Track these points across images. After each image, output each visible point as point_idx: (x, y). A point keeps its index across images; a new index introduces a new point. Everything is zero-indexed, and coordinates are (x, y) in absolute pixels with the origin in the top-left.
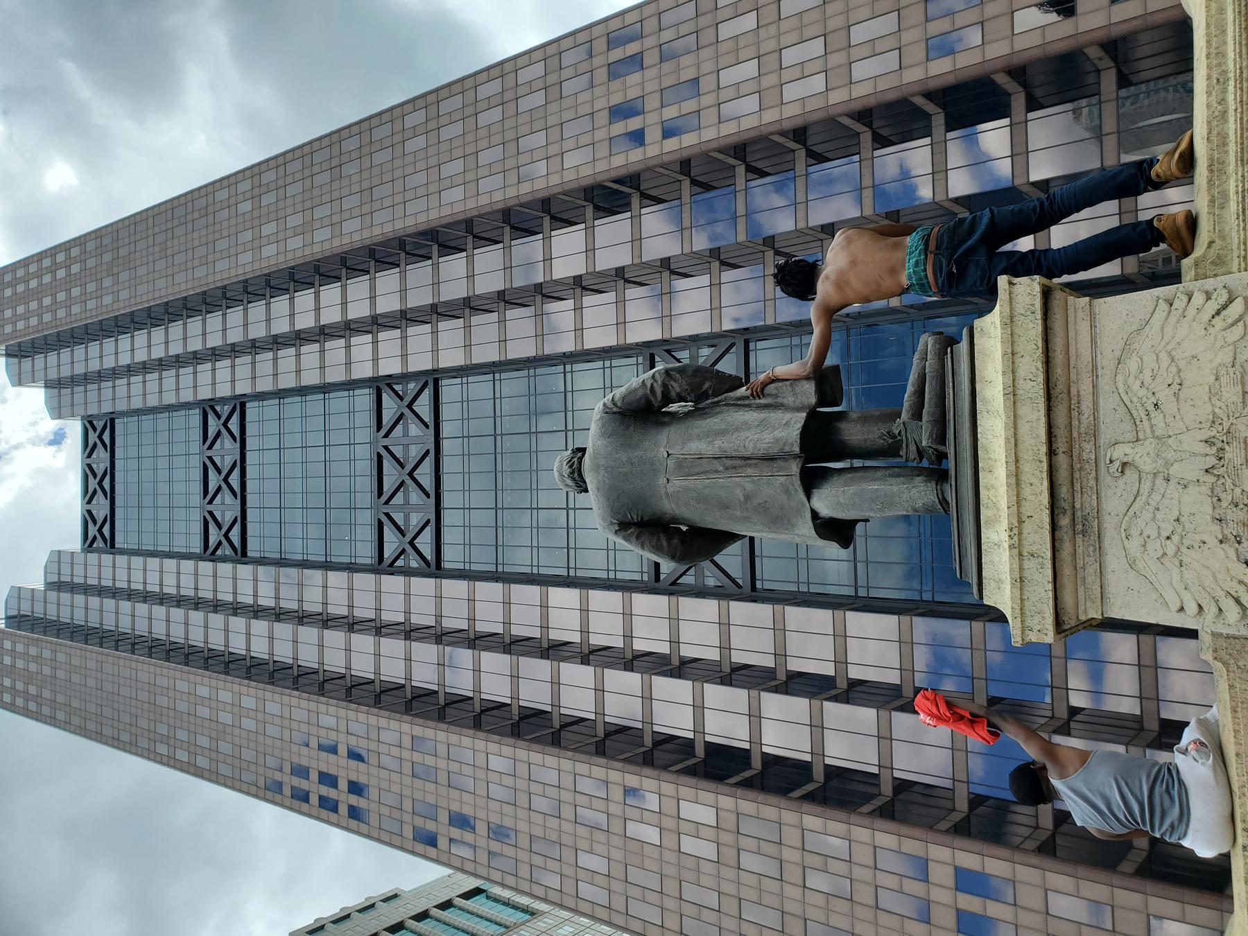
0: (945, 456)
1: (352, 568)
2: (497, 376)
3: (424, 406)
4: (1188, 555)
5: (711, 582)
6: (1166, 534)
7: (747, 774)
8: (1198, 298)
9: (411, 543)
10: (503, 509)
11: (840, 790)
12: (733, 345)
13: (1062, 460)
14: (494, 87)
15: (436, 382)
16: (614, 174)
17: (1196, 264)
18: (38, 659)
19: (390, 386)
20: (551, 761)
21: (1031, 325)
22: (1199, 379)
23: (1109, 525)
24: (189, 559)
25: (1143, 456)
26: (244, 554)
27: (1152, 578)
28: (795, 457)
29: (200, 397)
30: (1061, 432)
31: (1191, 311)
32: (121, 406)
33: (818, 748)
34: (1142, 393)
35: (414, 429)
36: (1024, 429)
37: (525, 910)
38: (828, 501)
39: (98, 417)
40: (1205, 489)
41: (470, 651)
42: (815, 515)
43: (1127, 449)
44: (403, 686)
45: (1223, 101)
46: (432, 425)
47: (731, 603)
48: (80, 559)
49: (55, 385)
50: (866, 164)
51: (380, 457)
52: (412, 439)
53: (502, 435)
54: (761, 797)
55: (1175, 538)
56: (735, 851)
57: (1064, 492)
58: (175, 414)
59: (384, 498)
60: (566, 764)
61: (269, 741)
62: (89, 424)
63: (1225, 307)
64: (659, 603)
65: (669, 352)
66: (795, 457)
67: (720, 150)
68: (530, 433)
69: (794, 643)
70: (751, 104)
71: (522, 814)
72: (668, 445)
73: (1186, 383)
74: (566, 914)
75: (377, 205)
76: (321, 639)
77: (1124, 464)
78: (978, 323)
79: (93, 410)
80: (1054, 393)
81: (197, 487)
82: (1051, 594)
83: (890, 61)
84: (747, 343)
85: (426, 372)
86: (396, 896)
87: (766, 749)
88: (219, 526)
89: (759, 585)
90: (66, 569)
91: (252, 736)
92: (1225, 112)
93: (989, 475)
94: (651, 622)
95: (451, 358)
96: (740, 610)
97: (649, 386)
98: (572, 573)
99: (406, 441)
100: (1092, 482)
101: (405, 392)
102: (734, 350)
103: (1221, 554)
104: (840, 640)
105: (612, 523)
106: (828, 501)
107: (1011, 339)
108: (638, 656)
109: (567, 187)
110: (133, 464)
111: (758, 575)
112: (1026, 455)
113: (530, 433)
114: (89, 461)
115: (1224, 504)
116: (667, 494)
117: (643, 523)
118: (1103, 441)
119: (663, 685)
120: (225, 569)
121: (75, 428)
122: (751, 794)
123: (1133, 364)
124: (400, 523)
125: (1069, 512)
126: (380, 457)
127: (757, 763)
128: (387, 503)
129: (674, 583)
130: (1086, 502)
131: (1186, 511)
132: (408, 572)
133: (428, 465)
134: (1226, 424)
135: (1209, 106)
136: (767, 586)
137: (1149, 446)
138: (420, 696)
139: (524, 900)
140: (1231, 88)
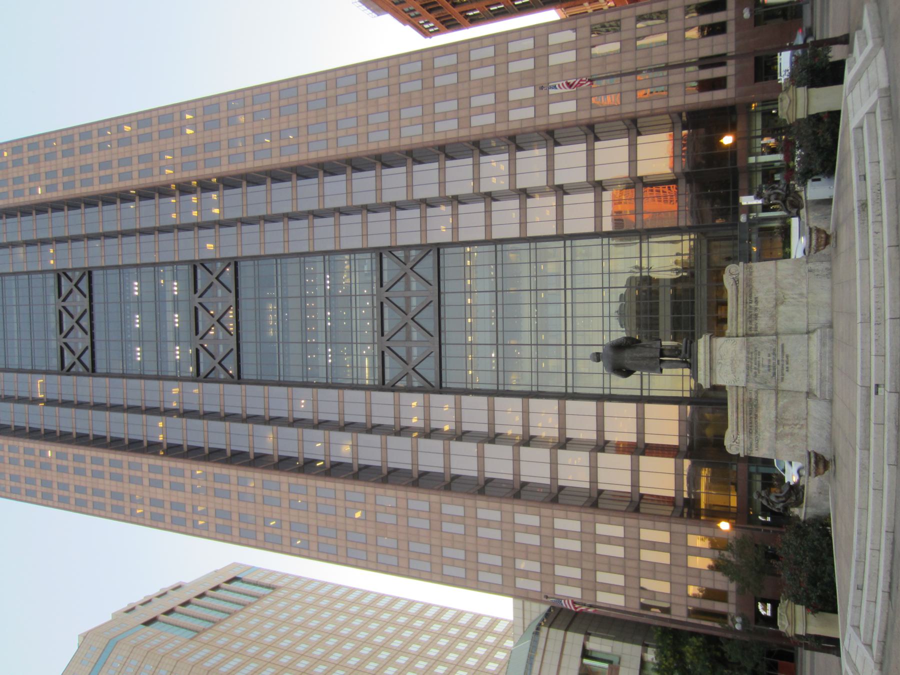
5: (416, 384)
14: (452, 59)
19: (203, 265)
26: (94, 370)
46: (88, 295)
51: (196, 309)
59: (64, 334)
67: (433, 147)
69: (376, 410)
70: (418, 130)
85: (85, 268)
89: (444, 385)
96: (435, 398)
104: (368, 405)
109: (340, 158)
111: (443, 380)
119: (310, 433)
126: (196, 309)
128: (201, 338)
129: (393, 386)
136: (449, 385)
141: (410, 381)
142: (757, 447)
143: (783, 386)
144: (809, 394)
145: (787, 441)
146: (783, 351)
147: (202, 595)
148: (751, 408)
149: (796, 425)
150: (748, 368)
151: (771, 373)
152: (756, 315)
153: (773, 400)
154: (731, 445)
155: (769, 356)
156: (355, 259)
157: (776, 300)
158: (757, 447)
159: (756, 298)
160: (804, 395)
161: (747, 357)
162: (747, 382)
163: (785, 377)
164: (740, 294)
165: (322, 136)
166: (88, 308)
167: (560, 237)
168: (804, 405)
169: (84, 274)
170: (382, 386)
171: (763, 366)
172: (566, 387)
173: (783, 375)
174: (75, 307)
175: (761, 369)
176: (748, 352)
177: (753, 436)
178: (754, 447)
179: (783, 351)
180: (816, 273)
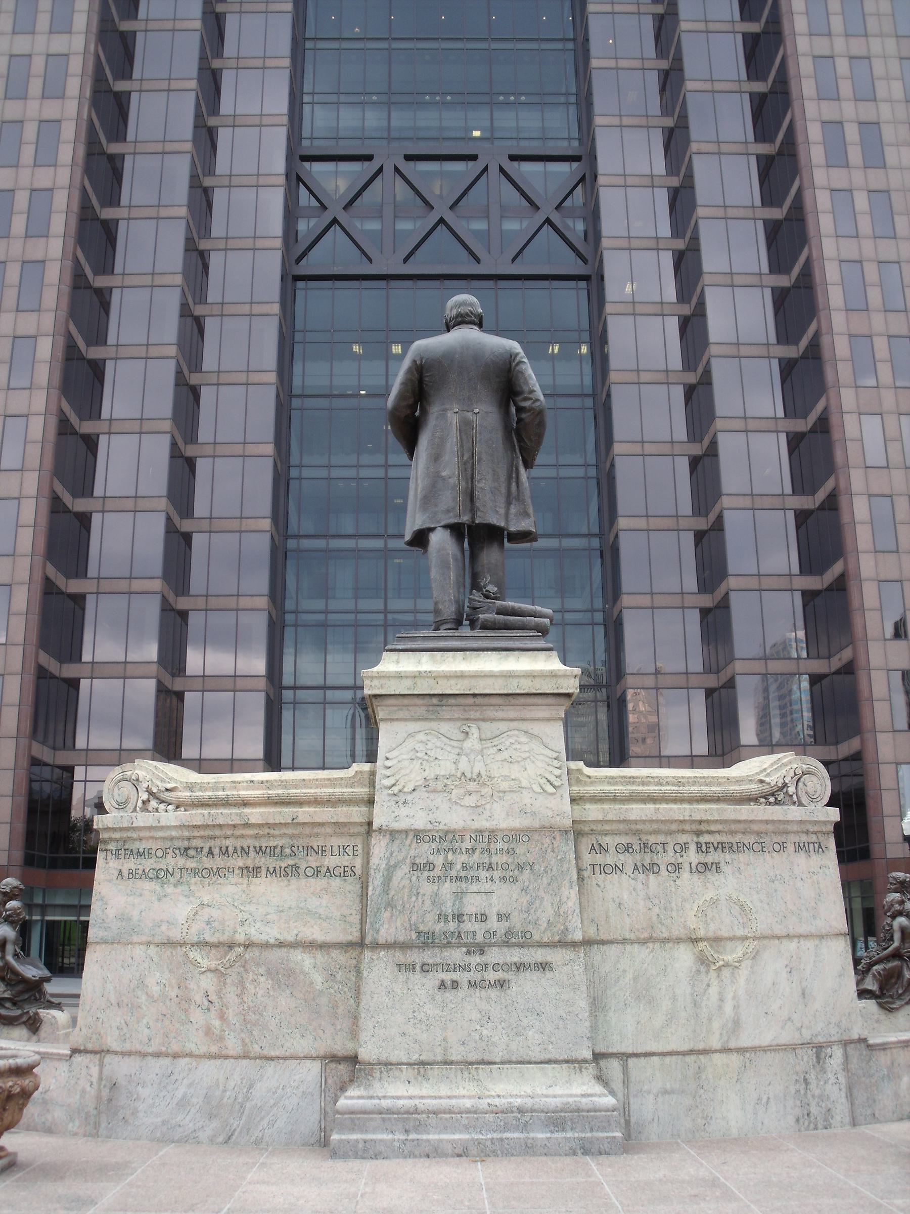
0: (473, 628)
2: (570, 45)
4: (417, 764)
6: (428, 752)
8: (558, 772)
12: (585, 261)
13: (471, 700)
16: (798, 125)
17: (579, 771)
21: (550, 686)
22: (515, 771)
23: (434, 725)
25: (472, 743)
27: (404, 745)
28: (473, 519)
30: (486, 700)
31: (551, 769)
34: (508, 743)
36: (490, 681)
38: (439, 539)
40: (453, 772)
42: (432, 530)
43: (476, 735)
45: (668, 783)
50: (771, 425)
54: (66, 289)
55: (426, 757)
57: (452, 701)
63: (551, 784)
64: (277, 162)
65: (582, 179)
66: (473, 519)
72: (485, 414)
73: (511, 765)
77: (467, 733)
78: (554, 654)
80: (510, 698)
82: (393, 693)
83: (875, 456)
84: (586, 278)
89: (301, 284)
92: (661, 785)
93: (461, 658)
97: (531, 396)
100: (456, 716)
103: (418, 778)
105: (421, 359)
106: (439, 539)
107: (542, 675)
112: (473, 682)
115: (445, 781)
116: (445, 410)
118: (481, 724)
122: (68, 278)
123: (524, 739)
125: (440, 703)
129: (299, 179)
130: (446, 712)
131: (442, 763)
134: (488, 783)
135: (667, 777)
137: (478, 746)
140: (674, 788)
142: (132, 874)
143: (379, 971)
144: (349, 1066)
145: (156, 980)
146: (519, 967)
148: (277, 851)
149: (222, 1017)
150: (448, 838)
151: (430, 924)
152: (652, 868)
153: (316, 933)
154: (136, 783)
155: (500, 917)
157: (716, 940)
158: (132, 874)
159: (717, 867)
160: (342, 1046)
161: (492, 834)
162: (393, 834)
163: (417, 977)
164: (731, 812)
167: (673, 455)
168: (302, 1045)
171: (459, 895)
173: (425, 968)
175: (447, 888)
176: (516, 836)
177: (172, 862)
178: (130, 864)
179: (519, 967)
180: (812, 1077)
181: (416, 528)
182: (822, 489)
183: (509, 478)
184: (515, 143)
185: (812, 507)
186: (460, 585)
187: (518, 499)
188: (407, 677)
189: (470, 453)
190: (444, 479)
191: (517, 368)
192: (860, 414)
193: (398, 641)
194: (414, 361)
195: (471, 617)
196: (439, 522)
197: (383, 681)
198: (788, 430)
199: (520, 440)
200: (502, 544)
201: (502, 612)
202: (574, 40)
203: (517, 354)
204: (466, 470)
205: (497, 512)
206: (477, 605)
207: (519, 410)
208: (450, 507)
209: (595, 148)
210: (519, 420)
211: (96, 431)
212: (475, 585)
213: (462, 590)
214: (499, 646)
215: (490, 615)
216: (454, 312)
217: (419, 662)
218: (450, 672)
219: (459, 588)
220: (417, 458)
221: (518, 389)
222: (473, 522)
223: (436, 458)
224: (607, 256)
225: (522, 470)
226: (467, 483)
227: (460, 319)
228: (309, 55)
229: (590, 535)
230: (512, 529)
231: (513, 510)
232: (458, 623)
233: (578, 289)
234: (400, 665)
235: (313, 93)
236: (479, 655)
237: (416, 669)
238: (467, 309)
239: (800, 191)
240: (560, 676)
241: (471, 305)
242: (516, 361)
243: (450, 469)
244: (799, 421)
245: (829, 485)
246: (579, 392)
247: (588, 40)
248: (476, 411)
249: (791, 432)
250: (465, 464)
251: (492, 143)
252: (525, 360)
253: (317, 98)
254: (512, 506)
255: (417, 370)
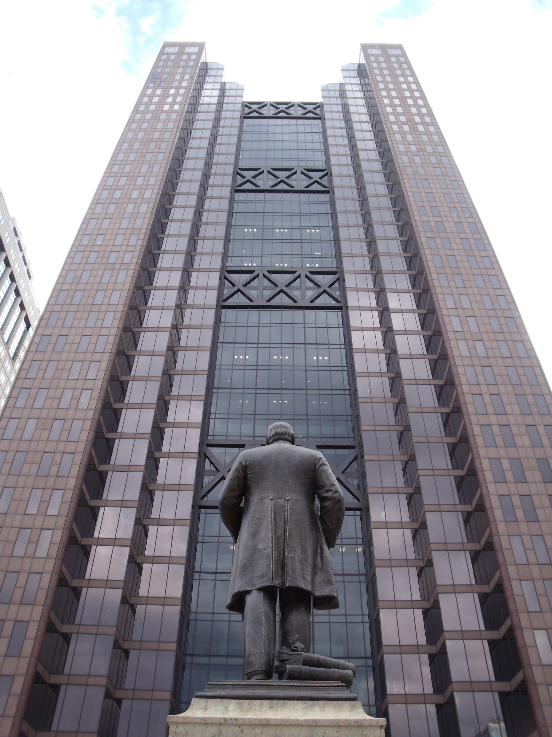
1: (225, 255)
2: (347, 392)
3: (325, 300)
5: (206, 480)
7: (88, 497)
9: (239, 290)
10: (258, 347)
11: (84, 515)
15: (340, 308)
16: (468, 427)
18: (174, 103)
19: (338, 280)
20: (101, 375)
24: (238, 141)
26: (237, 191)
28: (283, 582)
29: (333, 168)
32: (328, 124)
33: (124, 436)
35: (310, 294)
37: (16, 354)
38: (254, 600)
39: (322, 111)
41: (170, 326)
42: (248, 592)
44: (151, 285)
47: (206, 376)
48: (239, 100)
49: (342, 89)
51: (293, 272)
52: (304, 292)
53: (305, 348)
54: (73, 505)
56: (43, 487)
58: (323, 153)
60: (99, 384)
61: (124, 206)
62: (319, 106)
64: (194, 446)
65: (356, 458)
68: (304, 327)
69: (170, 495)
71: (71, 356)
72: (294, 500)
74: (13, 378)
75: (450, 277)
76: (192, 194)
79: (326, 108)
81: (279, 165)
86: (30, 277)
87: (102, 509)
88: (254, 177)
89: (203, 511)
90: (232, 93)
91: (128, 196)
93: (268, 707)
94: (180, 471)
95: (355, 319)
96: (187, 498)
97: (332, 488)
98: (219, 345)
99: (303, 288)
101: (334, 289)
102: (356, 501)
108: (174, 355)
110: (294, 129)
111: (209, 511)
113: (304, 327)
114: (296, 105)
116: (262, 498)
117: (244, 484)
120: (228, 180)
121: (317, 98)
122: (75, 499)
124: (252, 284)
126: (293, 272)
127: (110, 435)
129: (206, 456)
132: (221, 288)
133: (288, 302)
136: (202, 516)
138: (158, 242)
139: (22, 354)
141: (210, 473)
147: (17, 293)
156: (342, 371)
165: (481, 379)
166: (295, 189)
169: (338, 302)
170: (206, 444)
172: (192, 655)
174: (296, 180)
181: (236, 591)
182: (503, 626)
183: (315, 553)
184: (319, 439)
185: (498, 638)
186: (271, 641)
187: (322, 569)
188: (212, 724)
189: (283, 530)
190: (260, 551)
191: (321, 468)
192: (520, 580)
193: (208, 688)
194: (241, 463)
195: (280, 669)
196: (254, 586)
197: (188, 728)
198: (479, 591)
199: (324, 523)
200: (308, 609)
201: (308, 662)
202: (349, 390)
203: (320, 459)
204: (278, 544)
205: (304, 578)
206: (286, 657)
207: (323, 500)
208: (264, 573)
209: (362, 442)
210: (323, 508)
211: (81, 585)
212: (285, 642)
213: (272, 645)
214: (305, 695)
215: (297, 666)
216: (273, 432)
217: (226, 710)
218: (255, 719)
219: (269, 643)
220: (239, 541)
221: (322, 484)
222: (284, 585)
223: (254, 535)
224: (371, 497)
225: (325, 547)
226: (279, 554)
227: (277, 437)
228: (214, 396)
229: (366, 658)
230: (317, 594)
231: (319, 578)
232: (268, 675)
233: (355, 515)
234: (208, 712)
235: (215, 414)
236: (285, 704)
237: (222, 716)
238: (283, 430)
239: (472, 459)
240: (366, 727)
241: (285, 427)
242: (320, 463)
243: (265, 542)
244: (485, 586)
245: (508, 623)
246: (357, 573)
247: (356, 390)
248: (288, 498)
249: (481, 593)
250: (278, 538)
251: (308, 440)
252: (327, 463)
253: (217, 416)
254: (318, 576)
255: (242, 470)
